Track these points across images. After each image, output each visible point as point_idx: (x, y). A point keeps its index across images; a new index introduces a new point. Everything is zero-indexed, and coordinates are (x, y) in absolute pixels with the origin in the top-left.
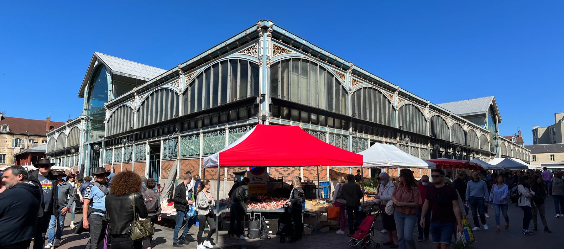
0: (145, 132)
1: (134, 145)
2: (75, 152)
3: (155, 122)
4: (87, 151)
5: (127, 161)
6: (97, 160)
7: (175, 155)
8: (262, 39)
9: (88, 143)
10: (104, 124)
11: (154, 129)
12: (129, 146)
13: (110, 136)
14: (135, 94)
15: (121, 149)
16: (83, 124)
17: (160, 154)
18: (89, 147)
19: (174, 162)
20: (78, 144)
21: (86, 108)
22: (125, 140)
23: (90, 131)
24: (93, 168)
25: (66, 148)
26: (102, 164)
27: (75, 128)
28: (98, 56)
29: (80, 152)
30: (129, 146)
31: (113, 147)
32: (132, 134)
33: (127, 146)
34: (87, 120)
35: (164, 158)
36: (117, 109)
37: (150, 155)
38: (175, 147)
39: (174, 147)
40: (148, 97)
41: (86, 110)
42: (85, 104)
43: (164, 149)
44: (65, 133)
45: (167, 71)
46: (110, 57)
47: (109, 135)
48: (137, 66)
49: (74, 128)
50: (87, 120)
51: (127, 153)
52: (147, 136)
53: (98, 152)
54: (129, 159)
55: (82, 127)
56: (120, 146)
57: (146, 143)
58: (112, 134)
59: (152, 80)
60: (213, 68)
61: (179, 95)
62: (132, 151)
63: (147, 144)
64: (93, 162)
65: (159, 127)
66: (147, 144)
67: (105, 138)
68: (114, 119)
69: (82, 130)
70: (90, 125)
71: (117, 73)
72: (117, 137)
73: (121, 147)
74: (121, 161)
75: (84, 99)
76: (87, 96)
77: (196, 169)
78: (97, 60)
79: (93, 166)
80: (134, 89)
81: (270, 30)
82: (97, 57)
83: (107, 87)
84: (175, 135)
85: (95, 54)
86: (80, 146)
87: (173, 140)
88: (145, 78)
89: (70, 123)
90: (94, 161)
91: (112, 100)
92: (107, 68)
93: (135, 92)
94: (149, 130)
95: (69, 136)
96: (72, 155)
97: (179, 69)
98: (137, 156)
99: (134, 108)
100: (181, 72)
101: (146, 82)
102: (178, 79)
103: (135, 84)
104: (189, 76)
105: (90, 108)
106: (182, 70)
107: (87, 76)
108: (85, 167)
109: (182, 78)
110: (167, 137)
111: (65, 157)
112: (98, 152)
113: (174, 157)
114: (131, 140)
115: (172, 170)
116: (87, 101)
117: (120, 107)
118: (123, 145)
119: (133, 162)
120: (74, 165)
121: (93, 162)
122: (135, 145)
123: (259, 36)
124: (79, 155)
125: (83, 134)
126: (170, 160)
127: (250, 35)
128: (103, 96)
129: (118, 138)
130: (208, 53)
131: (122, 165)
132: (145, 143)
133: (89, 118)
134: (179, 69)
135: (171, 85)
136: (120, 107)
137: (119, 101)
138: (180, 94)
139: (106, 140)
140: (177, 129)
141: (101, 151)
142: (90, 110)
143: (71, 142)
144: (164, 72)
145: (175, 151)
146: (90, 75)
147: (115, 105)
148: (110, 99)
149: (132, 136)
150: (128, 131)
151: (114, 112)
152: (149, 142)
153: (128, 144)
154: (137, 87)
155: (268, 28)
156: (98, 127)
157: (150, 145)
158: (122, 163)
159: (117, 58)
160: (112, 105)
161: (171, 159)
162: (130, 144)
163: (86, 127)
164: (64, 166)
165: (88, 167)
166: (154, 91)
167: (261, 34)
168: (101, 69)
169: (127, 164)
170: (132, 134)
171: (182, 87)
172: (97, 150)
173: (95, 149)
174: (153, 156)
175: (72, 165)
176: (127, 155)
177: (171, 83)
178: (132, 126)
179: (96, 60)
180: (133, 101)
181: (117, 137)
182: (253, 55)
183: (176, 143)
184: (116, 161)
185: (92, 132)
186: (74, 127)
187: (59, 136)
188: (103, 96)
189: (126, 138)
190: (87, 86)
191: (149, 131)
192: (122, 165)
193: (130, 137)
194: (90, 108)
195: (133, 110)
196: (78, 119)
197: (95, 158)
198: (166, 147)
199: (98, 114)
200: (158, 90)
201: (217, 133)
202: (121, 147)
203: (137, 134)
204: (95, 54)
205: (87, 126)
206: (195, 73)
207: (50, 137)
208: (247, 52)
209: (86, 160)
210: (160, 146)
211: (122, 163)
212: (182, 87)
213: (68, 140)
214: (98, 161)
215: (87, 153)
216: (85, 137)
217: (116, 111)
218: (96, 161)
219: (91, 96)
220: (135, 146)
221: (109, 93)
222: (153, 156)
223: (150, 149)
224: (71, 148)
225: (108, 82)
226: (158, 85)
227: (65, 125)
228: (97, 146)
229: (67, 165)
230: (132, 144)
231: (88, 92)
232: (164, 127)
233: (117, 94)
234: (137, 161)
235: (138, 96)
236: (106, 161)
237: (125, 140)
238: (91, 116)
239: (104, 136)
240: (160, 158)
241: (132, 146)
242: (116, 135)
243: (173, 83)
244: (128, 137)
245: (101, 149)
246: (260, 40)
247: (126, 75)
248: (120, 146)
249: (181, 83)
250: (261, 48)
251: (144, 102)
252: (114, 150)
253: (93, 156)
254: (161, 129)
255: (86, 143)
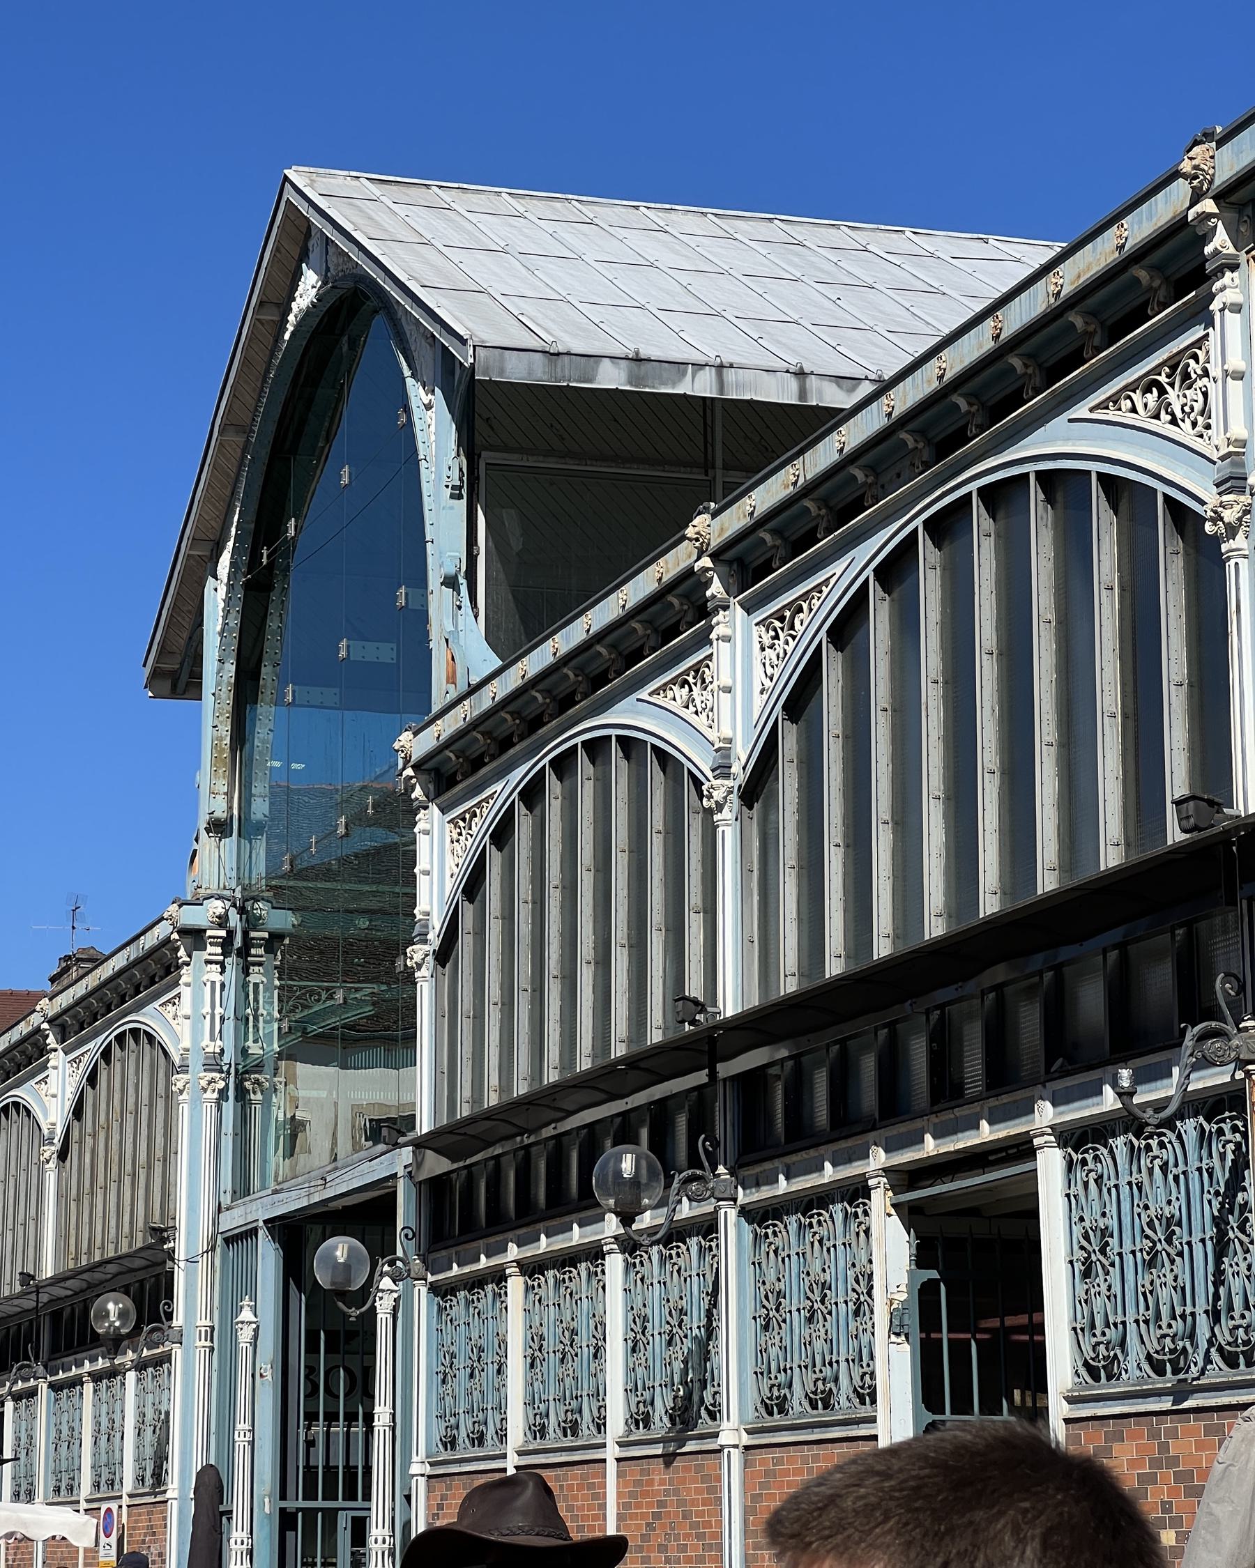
0: (842, 1042)
1: (729, 1216)
2: (137, 1330)
3: (897, 937)
4: (246, 1315)
5: (661, 1424)
6: (351, 1418)
7: (1223, 1336)
8: (1231, 296)
9: (259, 1210)
10: (409, 979)
11: (941, 1007)
12: (675, 1235)
13: (471, 1120)
14: (716, 588)
15: (596, 1276)
16: (196, 1002)
17: (1040, 1329)
18: (268, 1256)
19: (1220, 1434)
20: (161, 1234)
21: (221, 814)
22: (627, 1166)
23: (269, 1068)
24: (310, 1514)
25: (56, 1281)
26: (407, 1462)
27: (12, 1111)
28: (322, 203)
29: (178, 1321)
30: (675, 1235)
31: (80, 1364)
32: (701, 1077)
33: (652, 1231)
34: (238, 941)
35: (1093, 1373)
36: (532, 794)
37: (916, 1335)
38: (1220, 1222)
39: (1211, 1232)
40: (859, 603)
41: (219, 828)
42: (216, 760)
43: (635, 1342)
44: (164, 1036)
45: (1058, 247)
46: (438, 193)
47: (464, 1111)
48: (723, 254)
49: (116, 1049)
50: (238, 941)
51: (656, 1326)
52: (868, 1097)
53: (354, 1312)
54: (688, 1397)
55: (196, 1034)
56: (577, 1236)
57: (866, 1192)
58: (492, 1100)
59: (885, 387)
60: (938, 544)
61: (1216, 540)
62: (715, 1293)
63: (880, 1200)
64: (310, 1444)
65: (999, 973)
66: (880, 1200)
67: (420, 1145)
68: (508, 917)
69: (196, 1063)
70: (270, 1007)
71: (517, 371)
72: (548, 1132)
73: (595, 1253)
74: (600, 1426)
75: (200, 708)
76: (231, 669)
77: (792, 1536)
78: (316, 252)
79: (310, 1494)
80: (700, 522)
81: (210, 937)
82: (316, 220)
83: (423, 542)
84: (1206, 1063)
85: (289, 194)
86: (181, 1254)
87: (1189, 1127)
88: (813, 382)
89: (79, 990)
90: (319, 1429)
91: (473, 690)
92: (408, 328)
93: (706, 562)
94: (891, 1025)
95: (74, 1148)
96: (101, 1364)
97: (1196, 197)
98: (819, 1345)
99: (703, 762)
100: (716, 588)
101: (830, 419)
102: (1197, 332)
103: (708, 466)
104: (782, 619)
105: (260, 808)
106: (729, 563)
107: (221, 445)
108: (238, 1504)
109: (1237, 308)
110: (1109, 1100)
111: (43, 1388)
112: (354, 1312)
113: (1219, 1372)
114: (694, 1162)
115: (1200, 1535)
116: (225, 730)
117: (563, 765)
118: (611, 1225)
119: (731, 1432)
120: (128, 1485)
121: (310, 1444)
122: (745, 1212)
123: (1210, 267)
124: (166, 1358)
125: (208, 1111)
126: (1166, 1404)
127: (1092, 301)
128: (385, 653)
129: (558, 1137)
130: (941, 377)
131: (611, 1467)
132: (857, 1191)
133: (252, 922)
134: (1196, 197)
135: (1110, 415)
136: (563, 765)
137: (547, 692)
138: (1229, 516)
139: (437, 1164)
140: (1222, 987)
141: (383, 1307)
142: (259, 828)
143: (92, 1206)
144: (1025, 272)
145: (1219, 1273)
146: (246, 430)
147: (505, 744)
148: (452, 679)
149: (699, 1103)
150: (659, 1049)
151: (502, 834)
152: (903, 1178)
153: (662, 1203)
154: (730, 495)
155: (205, 931)
156: (351, 1016)
157: (911, 1215)
158: (612, 1452)
159: (505, 199)
160: (474, 752)
161: (1180, 1393)
162: (686, 1210)
163: (230, 1025)
164: (30, 1497)
165: (268, 1506)
166: (915, 520)
167: (1217, 252)
168: (353, 344)
169: (668, 1459)
170: (701, 1077)
171: (734, 729)
172: (342, 1294)
173: (323, 1278)
174: (960, 1352)
175: (107, 1481)
176: (658, 1342)
177: (1115, 399)
178: (694, 989)
179: (304, 256)
180: (696, 669)
181: (548, 1132)
182: (1185, 433)
183: (1222, 1177)
184: (542, 1431)
185: (290, 1080)
186: (120, 1038)
187: (92, 1079)
188: (385, 653)
189: (644, 1134)
190: (225, 560)
191: (844, 1053)
192: (611, 1467)
193: (682, 1122)
194: (260, 808)
195: (698, 784)
196: (149, 941)
197: (331, 1393)
198: (1106, 1232)
199: (343, 861)
200: (1025, 476)
201: (1179, 1137)
202: (595, 1253)
203: (752, 1082)
204: (289, 194)
205: (241, 1020)
206: (818, 589)
207: (94, 1046)
208: (1152, 398)
209: (242, 1426)
210: (1034, 1214)
211: (612, 1452)
212: (734, 729)
213: (62, 1196)
214: (358, 1429)
215: (245, 1335)
216: (228, 1144)
217: (520, 809)
218: (339, 1429)
219: (266, 671)
220: (747, 1227)
221: (440, 601)
222: (960, 1352)
223: (922, 1259)
224: (98, 1276)
225: (426, 489)
226: (961, 438)
227: (36, 1019)
228: (341, 1248)
229: (64, 1492)
230: (708, 1208)
231: (234, 622)
232: (1067, 970)
233: (524, 621)
234: (777, 1419)
235: (749, 608)
236: (439, 1430)
237: (627, 1166)
238: (279, 895)
239: (410, 1121)
240: (1040, 1385)
241: (708, 1227)
242: (526, 1102)
243: (1132, 387)
244: (660, 1114)
245: (386, 1283)
246: (1215, 306)
247: (611, 378)
248: (577, 1236)
249: (1239, 376)
250: (1226, 374)
251: (810, 676)
252: (515, 1285)
253: (311, 1370)
254: (1030, 991)
255: (232, 1221)
